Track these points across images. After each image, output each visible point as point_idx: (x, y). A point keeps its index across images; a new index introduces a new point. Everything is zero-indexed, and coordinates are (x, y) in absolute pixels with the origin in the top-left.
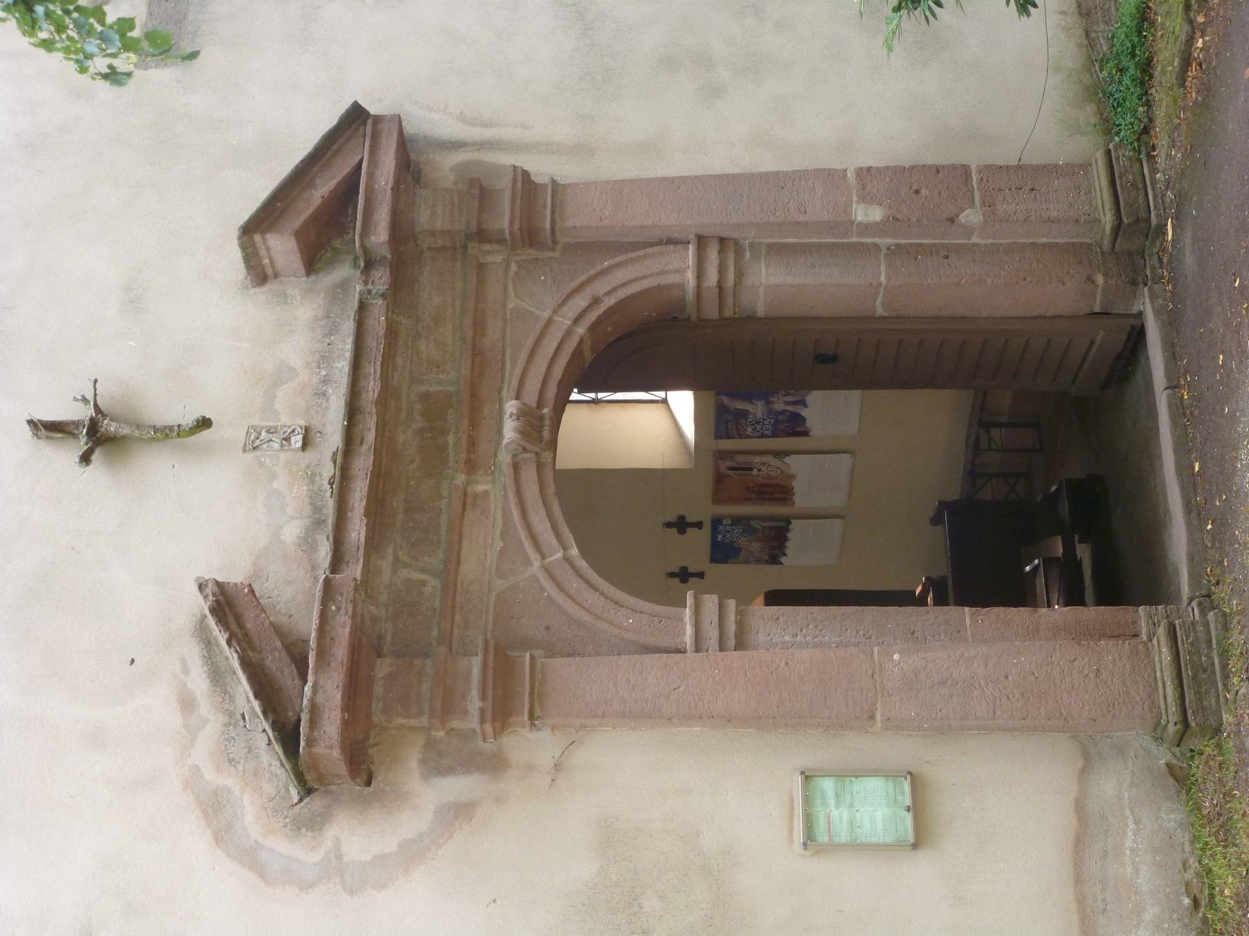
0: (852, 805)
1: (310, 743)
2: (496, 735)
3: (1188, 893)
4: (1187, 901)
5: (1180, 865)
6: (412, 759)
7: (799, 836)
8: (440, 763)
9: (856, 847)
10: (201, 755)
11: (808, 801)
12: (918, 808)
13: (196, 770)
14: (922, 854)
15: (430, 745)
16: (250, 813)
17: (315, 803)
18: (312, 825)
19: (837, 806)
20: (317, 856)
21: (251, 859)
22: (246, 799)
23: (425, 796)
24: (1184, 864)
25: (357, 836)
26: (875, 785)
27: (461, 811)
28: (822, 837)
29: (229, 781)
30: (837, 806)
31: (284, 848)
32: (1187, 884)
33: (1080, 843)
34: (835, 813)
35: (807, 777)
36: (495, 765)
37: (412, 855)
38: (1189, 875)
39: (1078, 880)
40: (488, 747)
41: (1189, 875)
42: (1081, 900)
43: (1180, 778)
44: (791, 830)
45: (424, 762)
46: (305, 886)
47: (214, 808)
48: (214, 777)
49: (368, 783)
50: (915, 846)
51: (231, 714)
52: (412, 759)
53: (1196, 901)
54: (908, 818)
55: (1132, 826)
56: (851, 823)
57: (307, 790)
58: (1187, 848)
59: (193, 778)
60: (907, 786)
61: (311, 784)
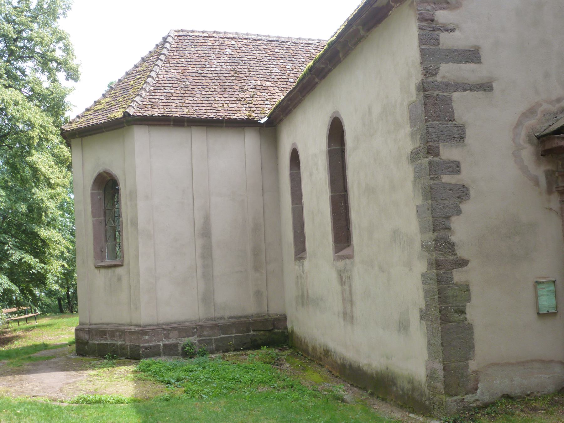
0: (547, 295)
1: (558, 138)
2: (558, 191)
3: (531, 393)
4: (529, 393)
5: (538, 390)
6: (549, 167)
7: (539, 280)
8: (549, 175)
9: (537, 297)
10: (545, 106)
11: (548, 282)
12: (548, 315)
13: (541, 105)
14: (536, 315)
15: (553, 172)
16: (531, 122)
17: (535, 141)
18: (530, 141)
19: (547, 291)
20: (522, 143)
21: (519, 124)
22: (535, 121)
23: (540, 172)
24: (539, 392)
25: (528, 153)
26: (554, 302)
27: (537, 183)
28: (539, 287)
29: (539, 115)
30: (547, 291)
31: (523, 133)
32: (533, 393)
33: (542, 361)
34: (545, 290)
35: (554, 282)
36: (550, 191)
37: (524, 169)
38: (536, 393)
39: (532, 361)
40: (554, 189)
41: (536, 393)
42: (527, 362)
43: (433, 417)
44: (539, 278)
45: (549, 170)
46: (514, 140)
47: (531, 112)
48: (540, 109)
49: (542, 155)
50: (538, 314)
51: (557, 114)
52: (549, 167)
53: (528, 395)
54: (546, 312)
55: (548, 376)
56: (543, 295)
57: (539, 138)
58: (543, 393)
59: (539, 105)
60: (554, 311)
61: (541, 139)
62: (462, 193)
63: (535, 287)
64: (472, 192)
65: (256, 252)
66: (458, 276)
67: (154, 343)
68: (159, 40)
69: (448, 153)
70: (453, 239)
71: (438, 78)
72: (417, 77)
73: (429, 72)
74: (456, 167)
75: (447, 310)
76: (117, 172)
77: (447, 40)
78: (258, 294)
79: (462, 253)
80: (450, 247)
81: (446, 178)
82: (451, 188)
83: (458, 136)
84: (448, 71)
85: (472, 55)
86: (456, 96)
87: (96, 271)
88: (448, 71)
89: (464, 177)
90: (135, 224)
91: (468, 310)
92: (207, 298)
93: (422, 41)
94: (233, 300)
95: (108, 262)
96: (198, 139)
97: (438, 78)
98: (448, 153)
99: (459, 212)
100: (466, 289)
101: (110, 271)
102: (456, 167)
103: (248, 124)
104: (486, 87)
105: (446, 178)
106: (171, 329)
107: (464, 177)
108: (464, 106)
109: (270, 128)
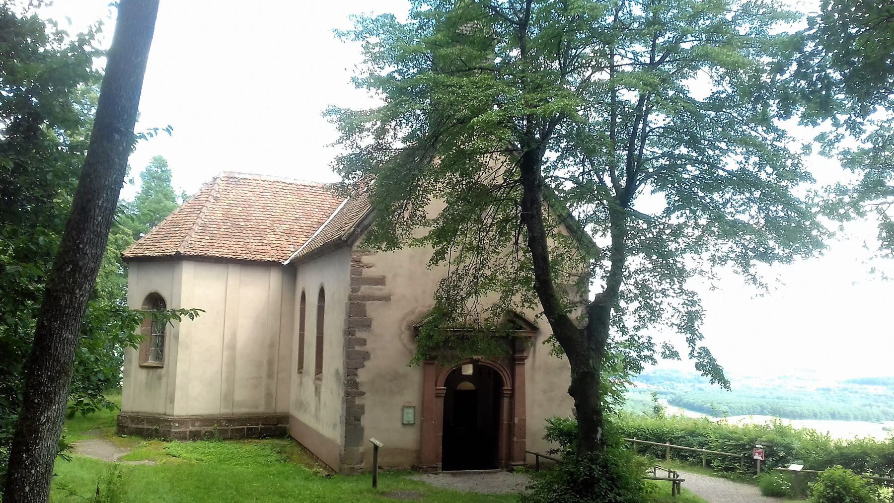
21: (403, 319)
25: (406, 335)
31: (404, 324)
37: (404, 345)
59: (416, 308)
62: (366, 356)
63: (403, 410)
64: (372, 356)
65: (270, 363)
66: (358, 401)
67: (182, 430)
68: (209, 180)
69: (359, 335)
70: (358, 380)
71: (359, 293)
72: (348, 292)
73: (354, 290)
74: (363, 342)
75: (353, 419)
76: (165, 294)
77: (366, 272)
78: (269, 395)
79: (362, 389)
80: (356, 385)
81: (357, 348)
82: (359, 353)
83: (367, 325)
84: (364, 289)
85: (381, 281)
86: (368, 303)
87: (141, 370)
88: (364, 289)
89: (368, 347)
90: (177, 337)
91: (362, 419)
92: (228, 397)
93: (352, 273)
94: (247, 400)
95: (151, 362)
96: (234, 275)
97: (359, 293)
98: (359, 335)
99: (363, 366)
100: (362, 408)
101: (151, 371)
102: (363, 342)
103: (276, 264)
104: (386, 299)
105: (357, 348)
106: (197, 420)
107: (368, 347)
108: (373, 310)
109: (291, 270)
